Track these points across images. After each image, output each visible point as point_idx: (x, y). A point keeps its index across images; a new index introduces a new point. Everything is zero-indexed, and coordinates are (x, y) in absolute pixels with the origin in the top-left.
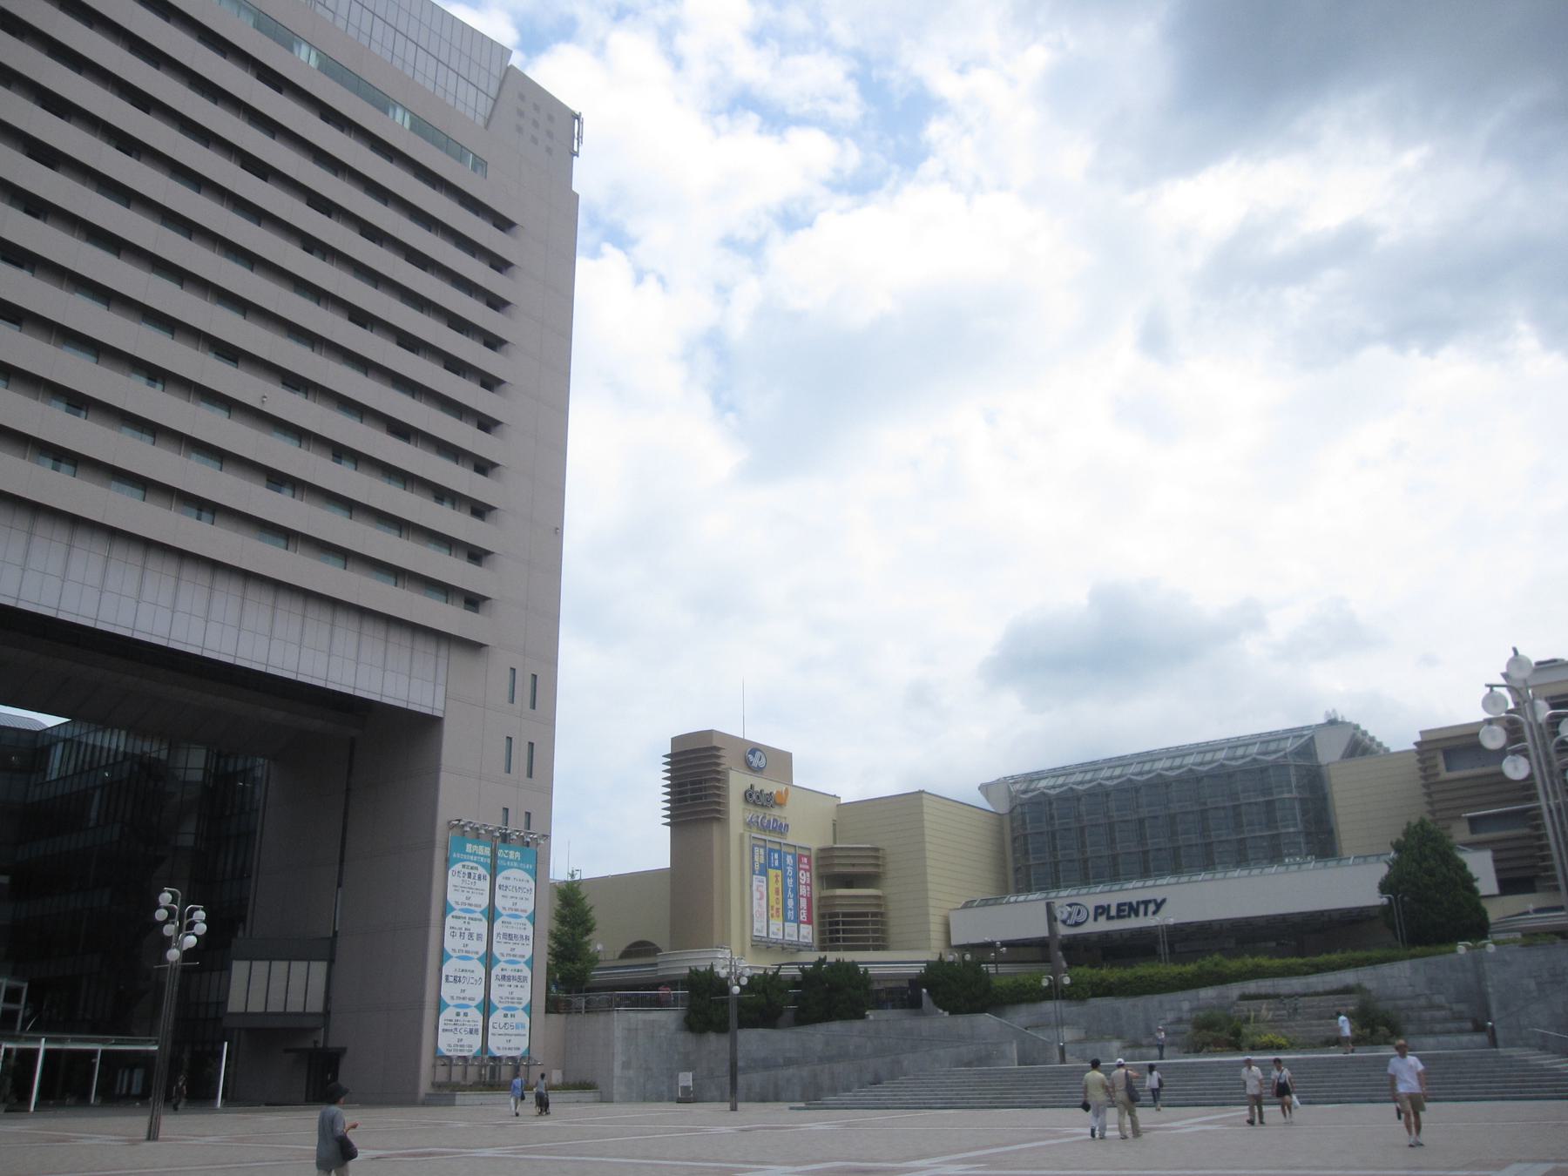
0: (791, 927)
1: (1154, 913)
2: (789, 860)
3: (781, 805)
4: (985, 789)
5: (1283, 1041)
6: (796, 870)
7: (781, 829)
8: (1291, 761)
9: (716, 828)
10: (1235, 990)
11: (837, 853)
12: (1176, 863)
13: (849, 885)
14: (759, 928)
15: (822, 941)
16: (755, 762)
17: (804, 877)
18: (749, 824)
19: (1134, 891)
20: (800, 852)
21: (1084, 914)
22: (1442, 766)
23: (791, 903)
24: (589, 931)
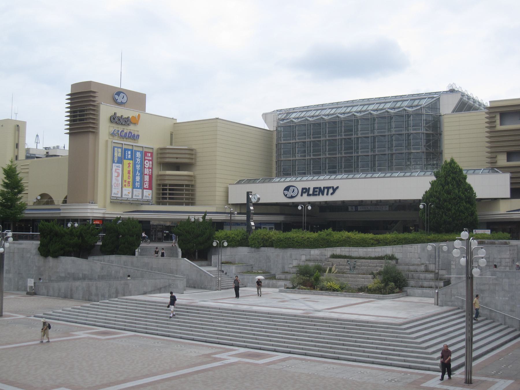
0: (138, 193)
1: (332, 194)
2: (138, 155)
3: (135, 124)
4: (265, 116)
5: (337, 287)
6: (143, 160)
7: (135, 137)
8: (424, 112)
9: (91, 137)
10: (329, 251)
11: (167, 151)
12: (350, 166)
13: (178, 169)
14: (116, 192)
15: (158, 198)
16: (119, 99)
17: (148, 164)
18: (113, 134)
19: (323, 181)
20: (147, 150)
21: (296, 191)
22: (498, 122)
23: (138, 178)
24: (20, 192)
